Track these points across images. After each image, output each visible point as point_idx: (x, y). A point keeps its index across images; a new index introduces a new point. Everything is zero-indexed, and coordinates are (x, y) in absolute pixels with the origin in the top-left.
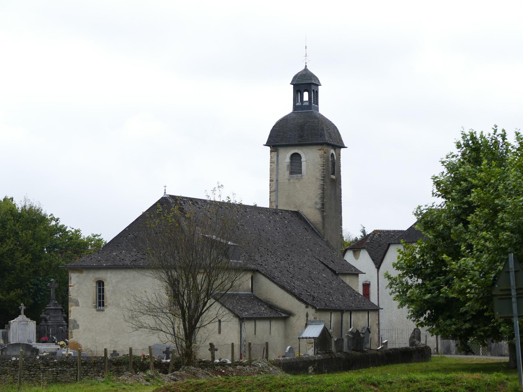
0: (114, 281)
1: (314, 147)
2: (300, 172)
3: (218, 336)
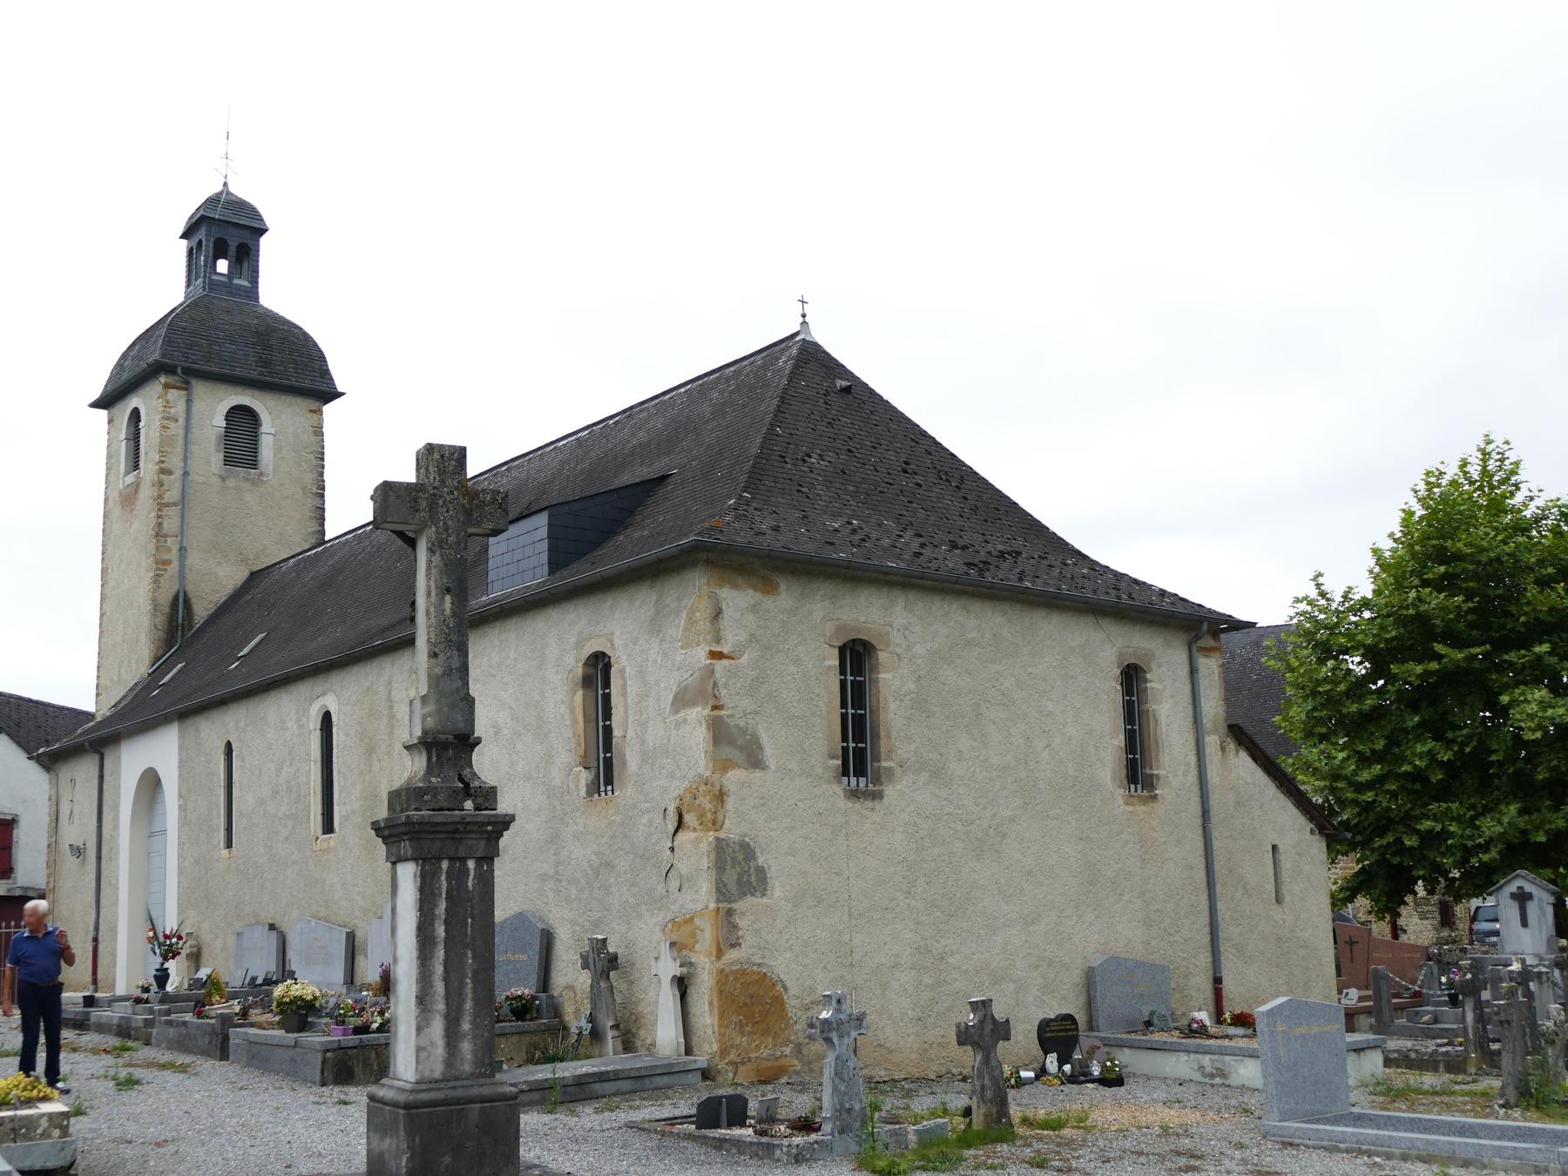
0: (919, 649)
1: (299, 400)
2: (253, 463)
3: (1277, 913)
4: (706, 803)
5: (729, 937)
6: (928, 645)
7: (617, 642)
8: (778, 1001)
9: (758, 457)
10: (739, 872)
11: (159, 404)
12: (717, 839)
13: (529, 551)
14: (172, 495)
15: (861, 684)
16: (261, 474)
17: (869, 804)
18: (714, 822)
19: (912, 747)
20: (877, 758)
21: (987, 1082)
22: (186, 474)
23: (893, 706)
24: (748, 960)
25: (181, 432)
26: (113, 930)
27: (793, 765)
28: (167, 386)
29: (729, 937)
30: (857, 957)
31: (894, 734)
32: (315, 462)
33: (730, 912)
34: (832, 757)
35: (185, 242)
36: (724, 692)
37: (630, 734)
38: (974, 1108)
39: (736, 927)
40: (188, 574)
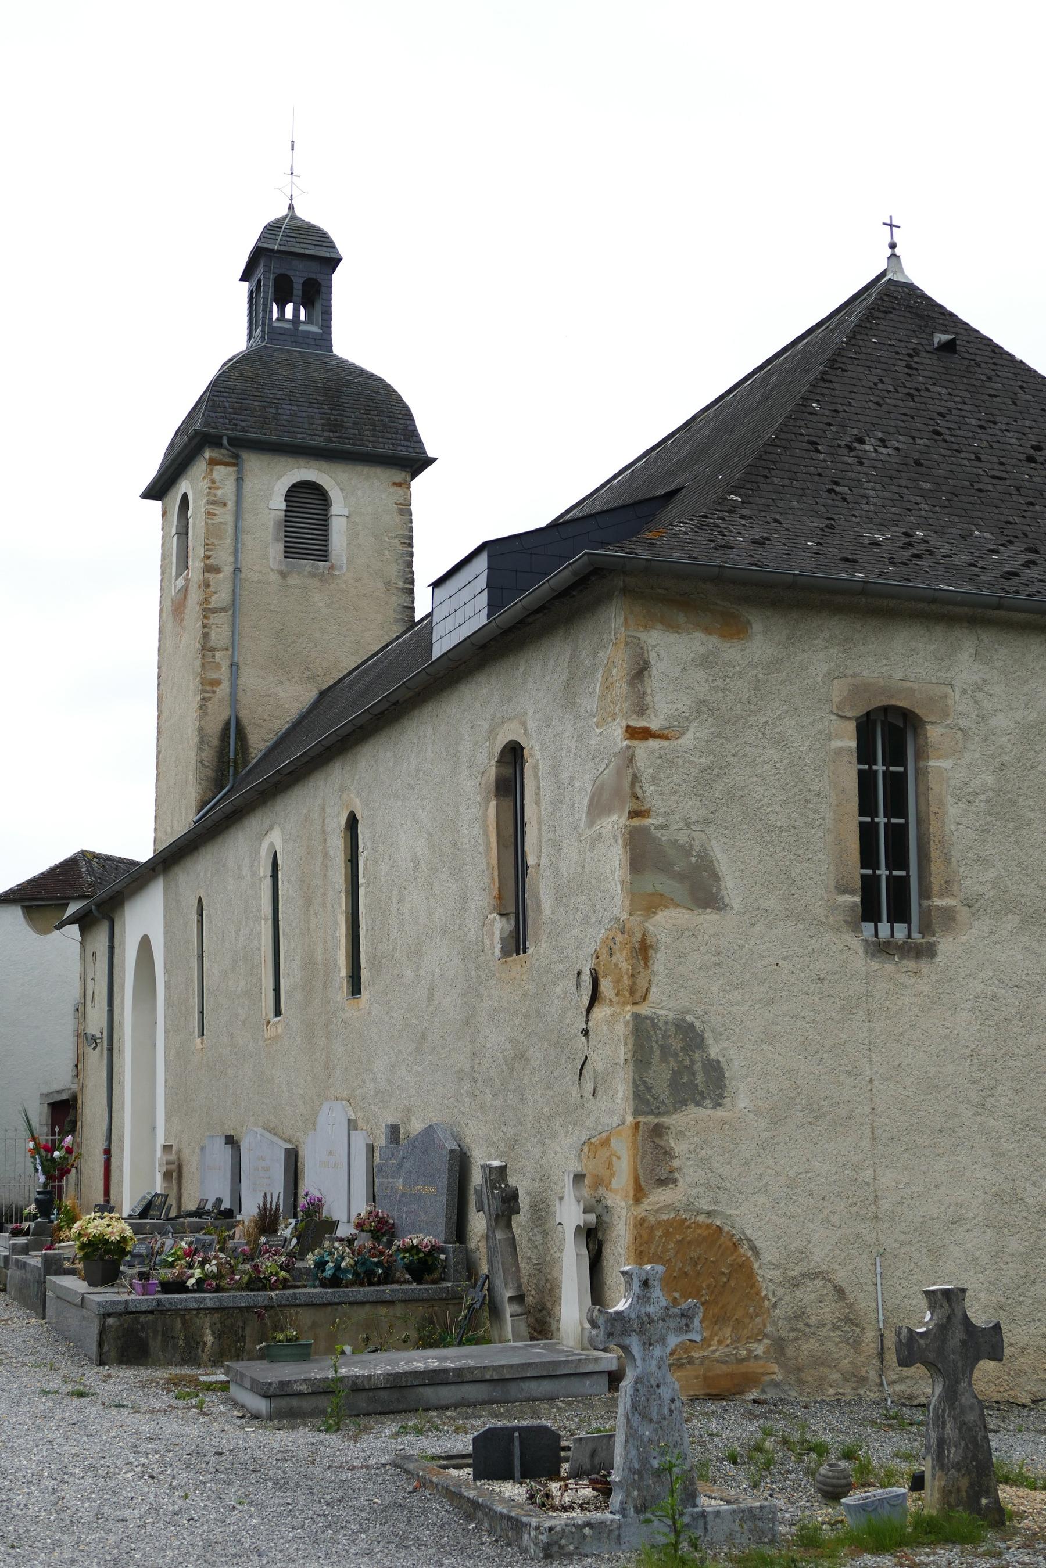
0: (1001, 721)
2: (323, 555)
4: (622, 960)
5: (656, 1166)
6: (1018, 715)
7: (531, 725)
8: (744, 1272)
9: (771, 443)
10: (676, 1069)
11: (204, 485)
12: (636, 1016)
13: (469, 610)
14: (221, 597)
15: (902, 778)
16: (332, 567)
17: (911, 964)
18: (632, 991)
19: (990, 875)
20: (925, 893)
21: (950, 1431)
22: (237, 570)
23: (953, 811)
24: (689, 1207)
25: (229, 519)
26: (121, 1140)
27: (771, 903)
28: (212, 462)
29: (656, 1166)
30: (885, 1205)
31: (955, 854)
32: (401, 549)
33: (658, 1131)
34: (844, 891)
35: (245, 285)
36: (650, 789)
37: (544, 861)
38: (928, 1477)
39: (668, 1153)
40: (241, 696)
